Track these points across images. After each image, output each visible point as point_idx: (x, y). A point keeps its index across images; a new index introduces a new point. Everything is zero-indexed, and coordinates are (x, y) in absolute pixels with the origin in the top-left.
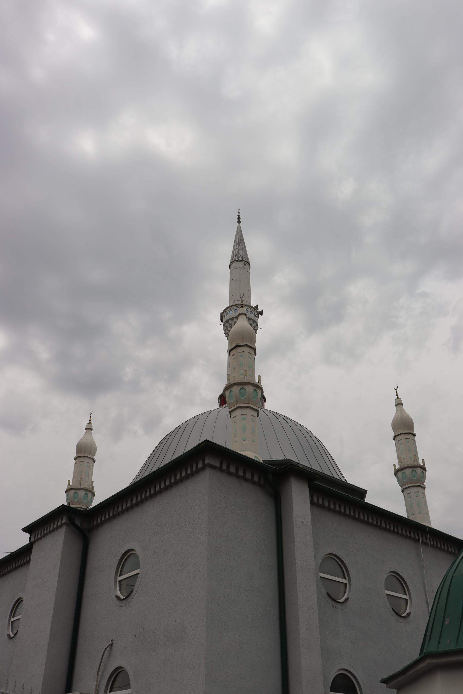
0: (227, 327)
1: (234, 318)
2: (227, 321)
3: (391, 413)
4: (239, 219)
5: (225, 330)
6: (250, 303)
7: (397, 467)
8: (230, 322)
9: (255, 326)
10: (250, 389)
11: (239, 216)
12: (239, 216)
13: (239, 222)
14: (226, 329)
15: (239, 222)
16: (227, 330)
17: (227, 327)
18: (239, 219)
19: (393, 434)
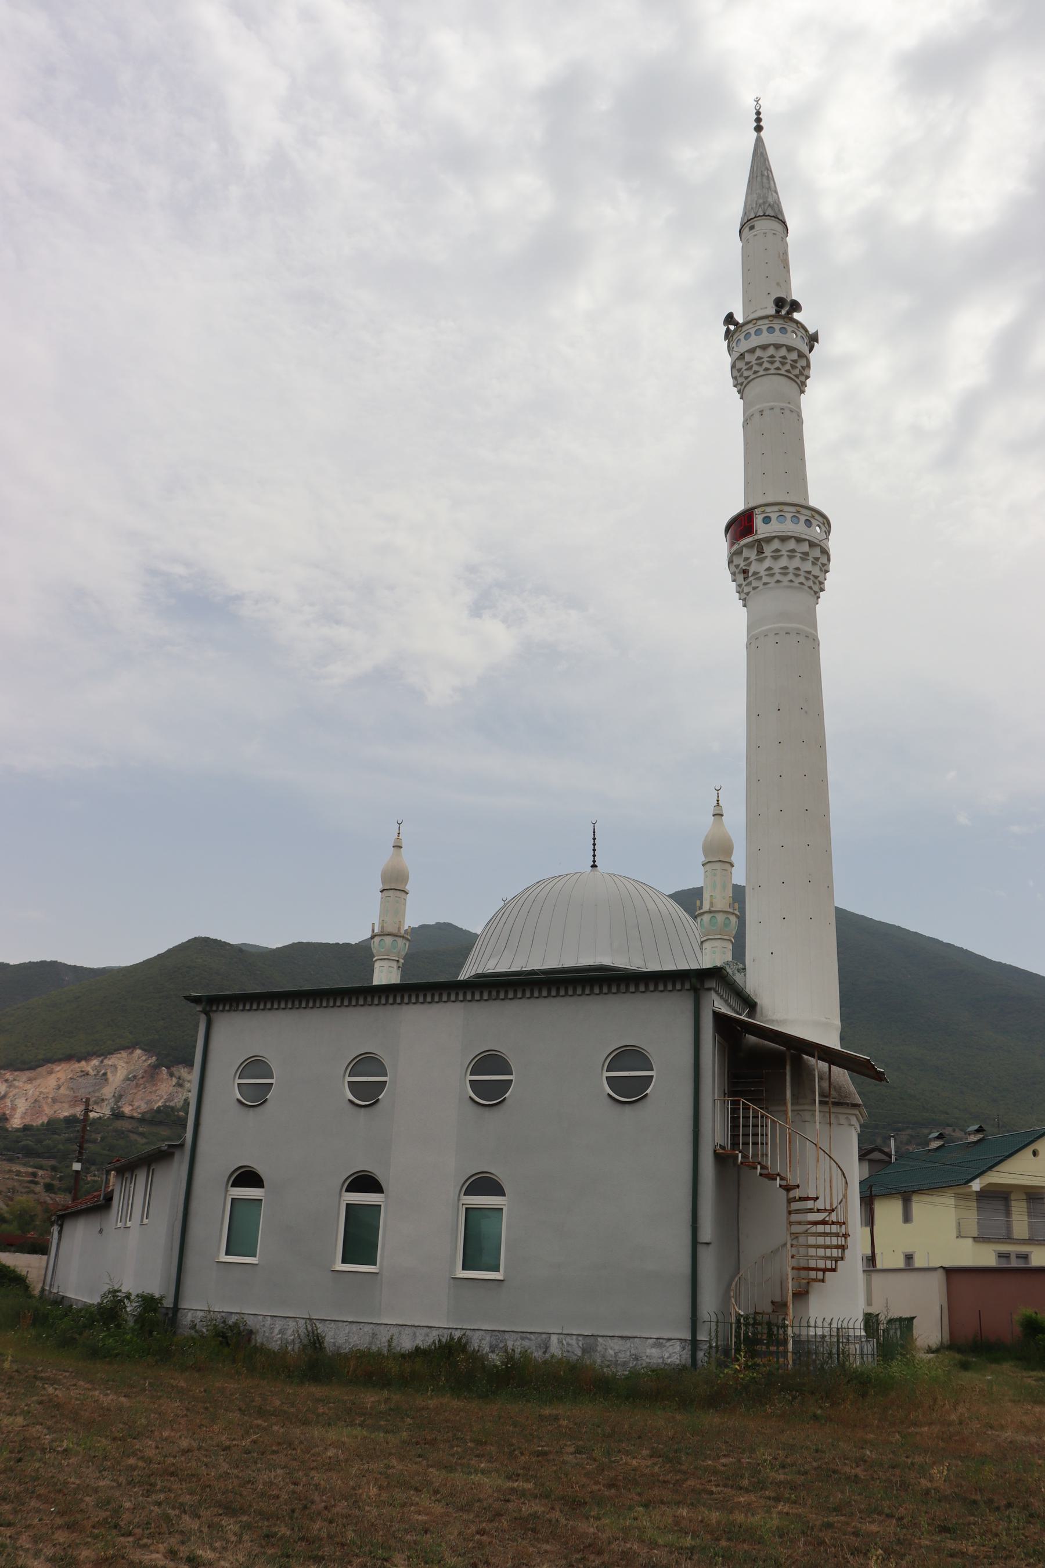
0: (739, 370)
1: (769, 345)
2: (742, 356)
3: (384, 856)
4: (758, 120)
5: (735, 378)
6: (806, 498)
7: (376, 931)
8: (748, 357)
9: (826, 562)
10: (816, 553)
11: (758, 113)
12: (758, 113)
13: (759, 129)
14: (736, 373)
15: (759, 129)
16: (741, 376)
17: (739, 370)
18: (758, 120)
19: (381, 887)
